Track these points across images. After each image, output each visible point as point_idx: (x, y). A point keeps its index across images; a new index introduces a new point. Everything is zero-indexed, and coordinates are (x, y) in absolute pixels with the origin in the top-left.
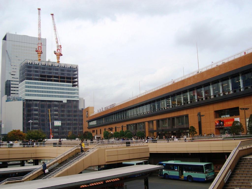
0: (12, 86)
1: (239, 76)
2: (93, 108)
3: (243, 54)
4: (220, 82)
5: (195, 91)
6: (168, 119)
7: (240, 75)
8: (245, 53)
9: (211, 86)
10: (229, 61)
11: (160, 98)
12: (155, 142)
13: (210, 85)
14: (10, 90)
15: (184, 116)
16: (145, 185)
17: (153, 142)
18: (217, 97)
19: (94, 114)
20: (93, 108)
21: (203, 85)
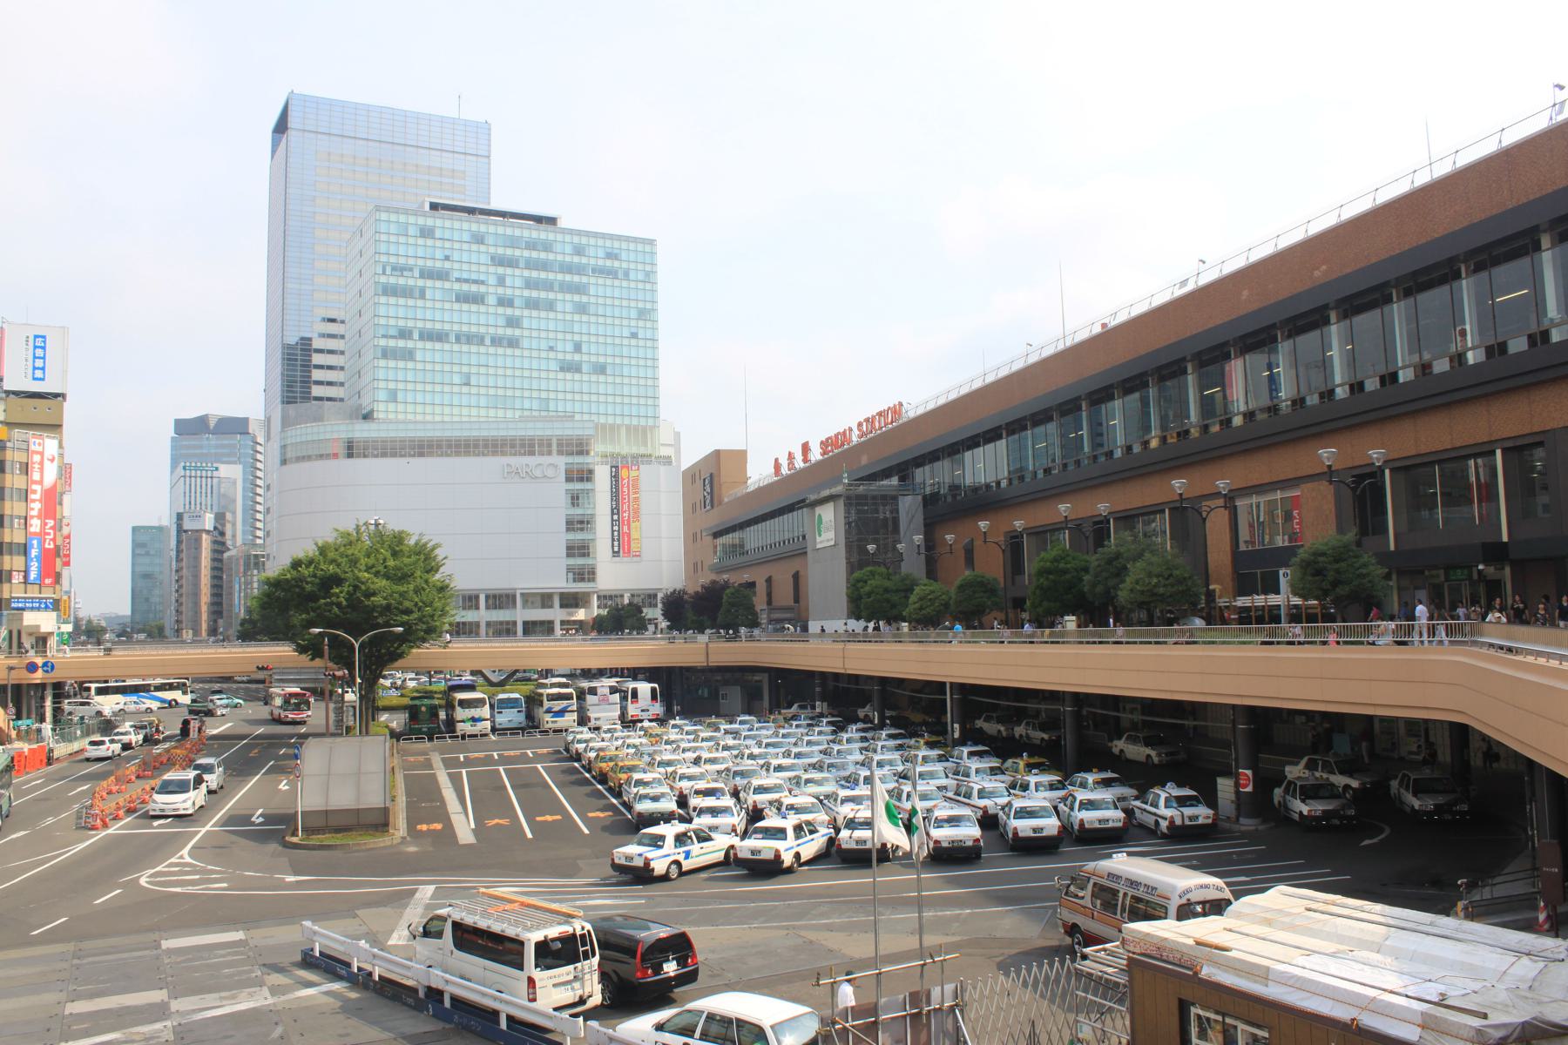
0: (317, 375)
1: (1537, 247)
2: (741, 456)
3: (1097, 329)
4: (1399, 300)
5: (1284, 347)
6: (1504, 451)
7: (1190, 370)
8: (1104, 325)
9: (1334, 328)
10: (1504, 144)
11: (1028, 412)
12: (1362, 643)
13: (1457, 276)
14: (307, 382)
15: (1493, 453)
16: (174, 466)
17: (1346, 643)
18: (1313, 406)
19: (751, 489)
20: (741, 456)
21: (1398, 282)
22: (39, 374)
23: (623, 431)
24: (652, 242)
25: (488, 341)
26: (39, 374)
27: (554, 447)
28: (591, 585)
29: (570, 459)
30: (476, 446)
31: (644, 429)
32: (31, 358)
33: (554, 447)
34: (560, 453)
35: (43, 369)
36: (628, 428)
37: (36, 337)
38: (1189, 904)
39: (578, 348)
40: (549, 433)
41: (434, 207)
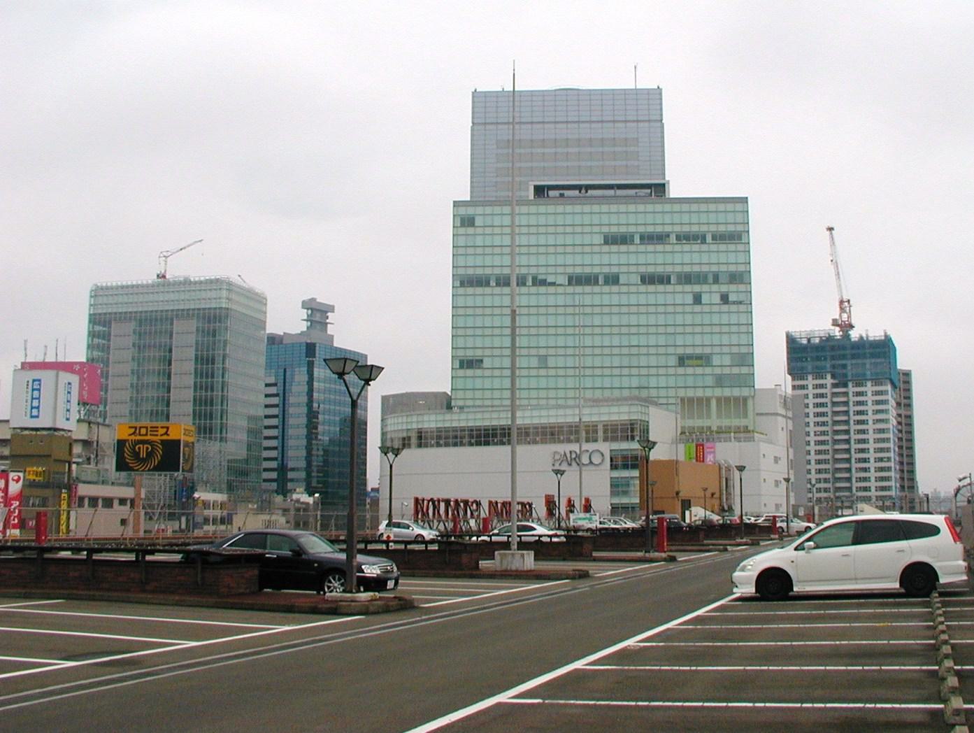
22: (35, 412)
23: (714, 403)
24: (744, 200)
25: (709, 239)
26: (35, 412)
27: (601, 434)
28: (584, 440)
29: (616, 446)
30: (494, 435)
31: (745, 399)
32: (30, 398)
33: (601, 434)
34: (606, 439)
35: (38, 408)
36: (719, 400)
37: (34, 381)
38: (739, 428)
39: (697, 299)
40: (595, 419)
41: (540, 191)
